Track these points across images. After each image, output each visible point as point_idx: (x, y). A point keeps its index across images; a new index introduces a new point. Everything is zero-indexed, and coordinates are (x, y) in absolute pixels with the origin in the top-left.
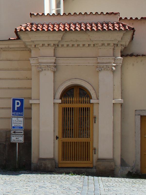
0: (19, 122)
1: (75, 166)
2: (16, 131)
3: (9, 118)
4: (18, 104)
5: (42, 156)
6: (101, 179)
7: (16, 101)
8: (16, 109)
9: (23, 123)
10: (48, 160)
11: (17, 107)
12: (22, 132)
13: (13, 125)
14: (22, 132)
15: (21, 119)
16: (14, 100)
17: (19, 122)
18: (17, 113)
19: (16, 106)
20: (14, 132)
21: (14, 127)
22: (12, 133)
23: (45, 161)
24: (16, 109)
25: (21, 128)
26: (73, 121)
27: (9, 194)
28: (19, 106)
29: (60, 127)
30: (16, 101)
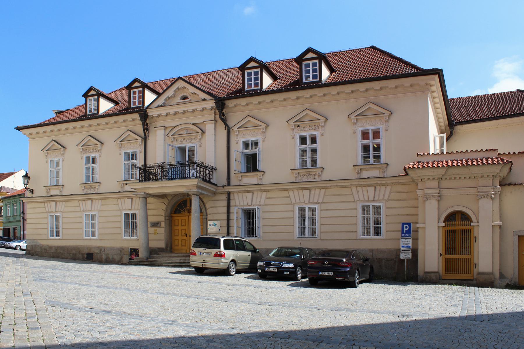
4: (406, 227)
7: (405, 226)
13: (402, 245)
15: (410, 240)
16: (403, 225)
19: (405, 229)
21: (403, 247)
25: (409, 247)
28: (407, 229)
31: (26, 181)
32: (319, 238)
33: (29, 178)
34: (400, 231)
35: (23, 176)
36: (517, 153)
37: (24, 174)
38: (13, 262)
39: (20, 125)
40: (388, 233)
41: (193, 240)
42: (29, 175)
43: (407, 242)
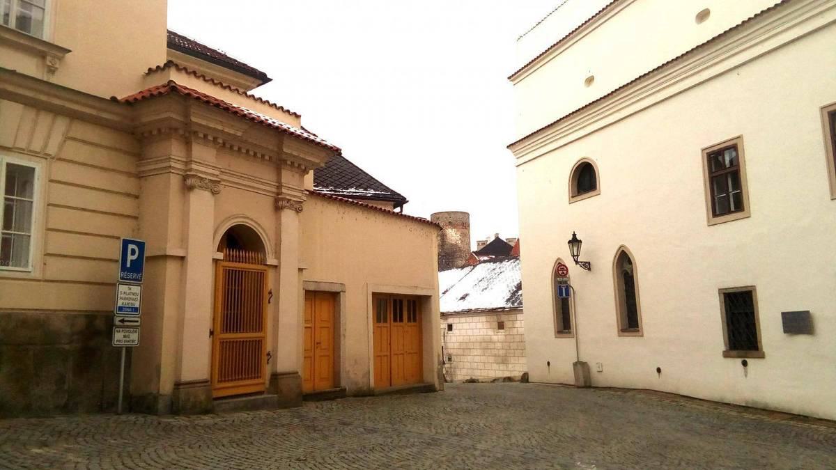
0: (131, 296)
1: (233, 394)
2: (126, 319)
3: (115, 285)
4: (133, 252)
5: (187, 376)
6: (396, 356)
7: (131, 246)
8: (128, 265)
9: (139, 298)
10: (199, 385)
11: (131, 261)
12: (137, 321)
13: (120, 304)
14: (137, 321)
15: (136, 289)
16: (126, 243)
17: (131, 296)
18: (131, 275)
19: (130, 258)
20: (122, 321)
21: (121, 309)
22: (118, 323)
23: (194, 387)
24: (128, 265)
25: (136, 309)
26: (229, 278)
27: (767, 468)
28: (135, 257)
29: (268, 242)
30: (131, 246)
31: (575, 249)
32: (36, 274)
33: (581, 241)
34: (117, 261)
35: (569, 242)
36: (162, 65)
37: (570, 238)
38: (594, 391)
39: (304, 127)
40: (50, 260)
41: (746, 359)
42: (578, 238)
43: (129, 294)
